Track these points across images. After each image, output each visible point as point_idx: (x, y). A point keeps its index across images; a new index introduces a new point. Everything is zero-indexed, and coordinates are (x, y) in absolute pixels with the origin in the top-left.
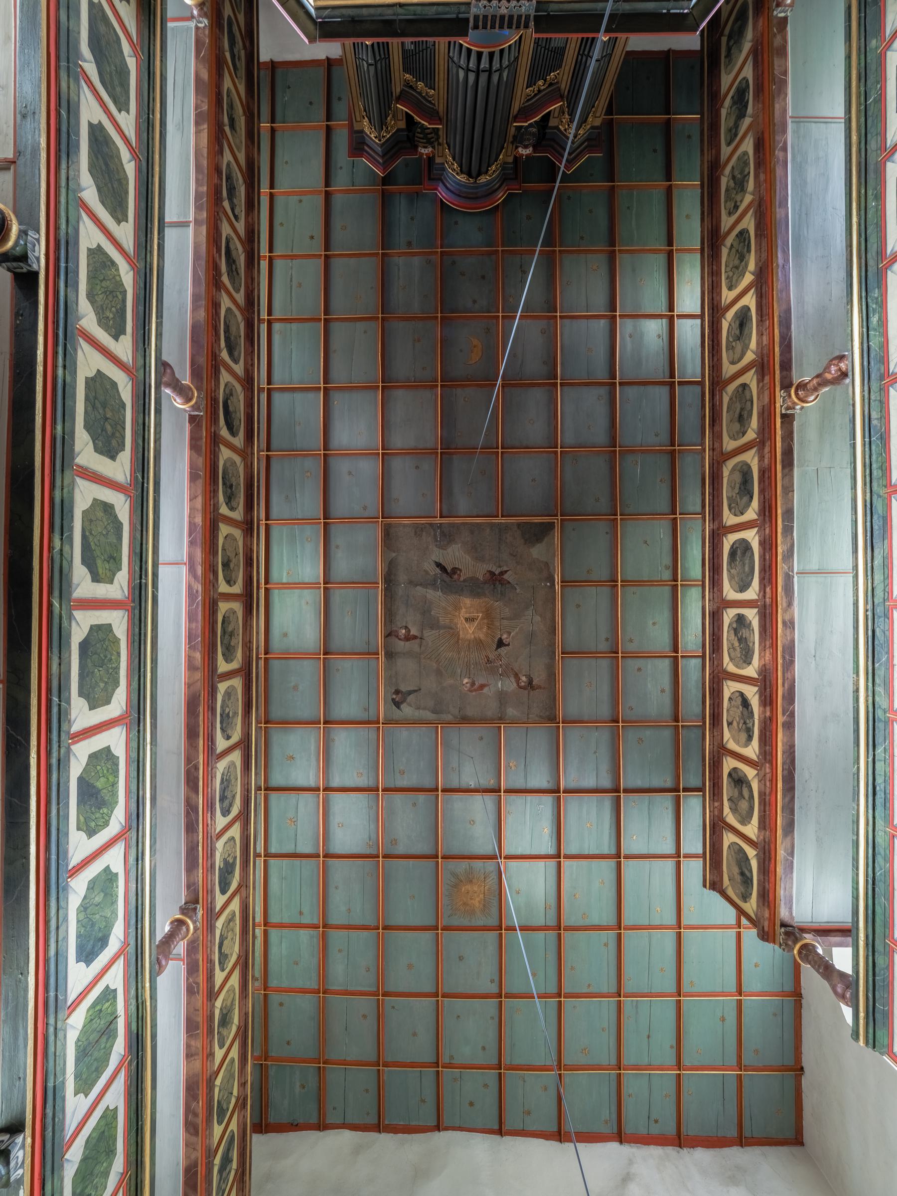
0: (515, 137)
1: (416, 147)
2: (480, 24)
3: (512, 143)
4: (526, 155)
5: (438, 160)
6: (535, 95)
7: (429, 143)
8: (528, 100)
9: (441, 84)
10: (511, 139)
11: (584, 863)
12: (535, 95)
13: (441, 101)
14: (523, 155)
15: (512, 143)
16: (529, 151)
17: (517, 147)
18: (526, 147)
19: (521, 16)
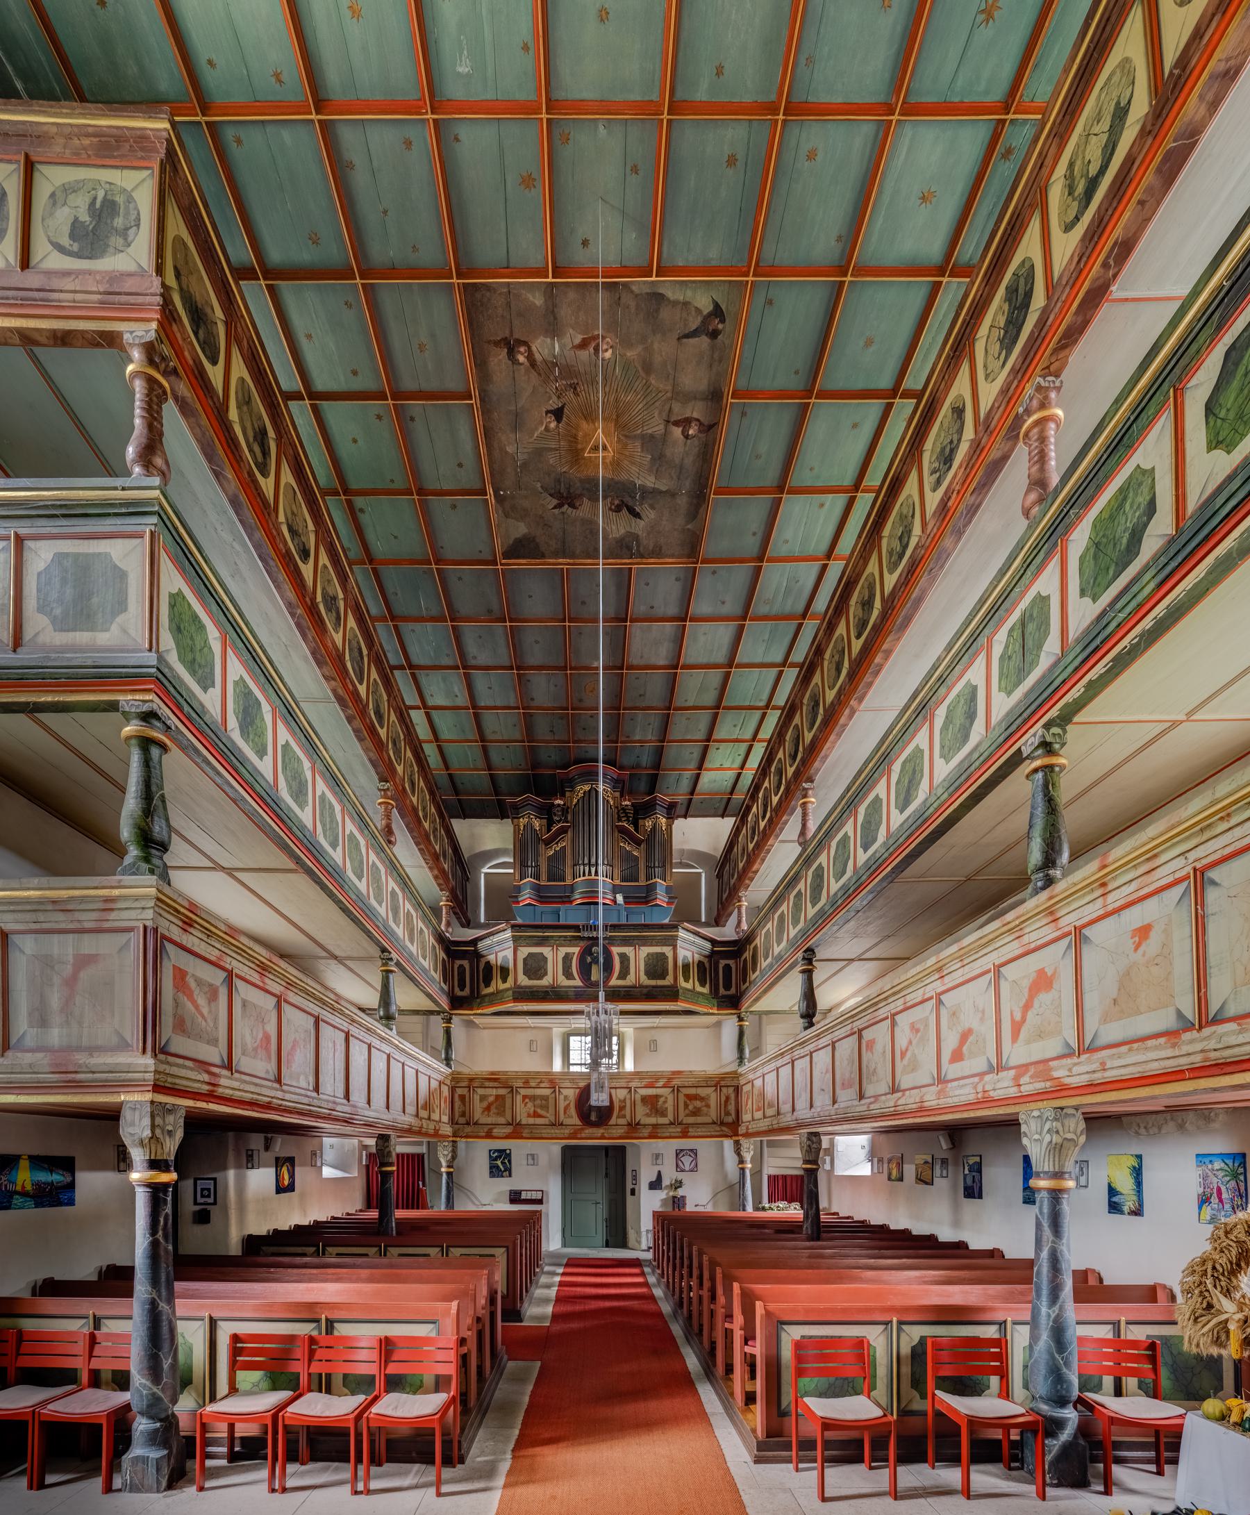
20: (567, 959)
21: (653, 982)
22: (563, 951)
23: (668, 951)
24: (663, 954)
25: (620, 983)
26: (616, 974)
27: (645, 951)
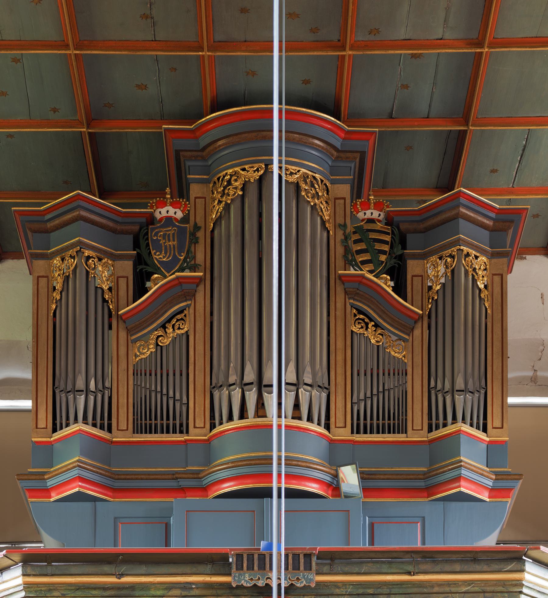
0: (195, 240)
1: (389, 221)
2: (302, 560)
3: (197, 228)
4: (164, 205)
5: (344, 190)
6: (169, 321)
7: (363, 232)
8: (181, 312)
9: (340, 344)
10: (200, 234)
11: (398, 524)
12: (169, 321)
13: (340, 313)
14: (173, 205)
15: (197, 228)
16: (163, 212)
17: (185, 219)
18: (169, 220)
19: (248, 569)
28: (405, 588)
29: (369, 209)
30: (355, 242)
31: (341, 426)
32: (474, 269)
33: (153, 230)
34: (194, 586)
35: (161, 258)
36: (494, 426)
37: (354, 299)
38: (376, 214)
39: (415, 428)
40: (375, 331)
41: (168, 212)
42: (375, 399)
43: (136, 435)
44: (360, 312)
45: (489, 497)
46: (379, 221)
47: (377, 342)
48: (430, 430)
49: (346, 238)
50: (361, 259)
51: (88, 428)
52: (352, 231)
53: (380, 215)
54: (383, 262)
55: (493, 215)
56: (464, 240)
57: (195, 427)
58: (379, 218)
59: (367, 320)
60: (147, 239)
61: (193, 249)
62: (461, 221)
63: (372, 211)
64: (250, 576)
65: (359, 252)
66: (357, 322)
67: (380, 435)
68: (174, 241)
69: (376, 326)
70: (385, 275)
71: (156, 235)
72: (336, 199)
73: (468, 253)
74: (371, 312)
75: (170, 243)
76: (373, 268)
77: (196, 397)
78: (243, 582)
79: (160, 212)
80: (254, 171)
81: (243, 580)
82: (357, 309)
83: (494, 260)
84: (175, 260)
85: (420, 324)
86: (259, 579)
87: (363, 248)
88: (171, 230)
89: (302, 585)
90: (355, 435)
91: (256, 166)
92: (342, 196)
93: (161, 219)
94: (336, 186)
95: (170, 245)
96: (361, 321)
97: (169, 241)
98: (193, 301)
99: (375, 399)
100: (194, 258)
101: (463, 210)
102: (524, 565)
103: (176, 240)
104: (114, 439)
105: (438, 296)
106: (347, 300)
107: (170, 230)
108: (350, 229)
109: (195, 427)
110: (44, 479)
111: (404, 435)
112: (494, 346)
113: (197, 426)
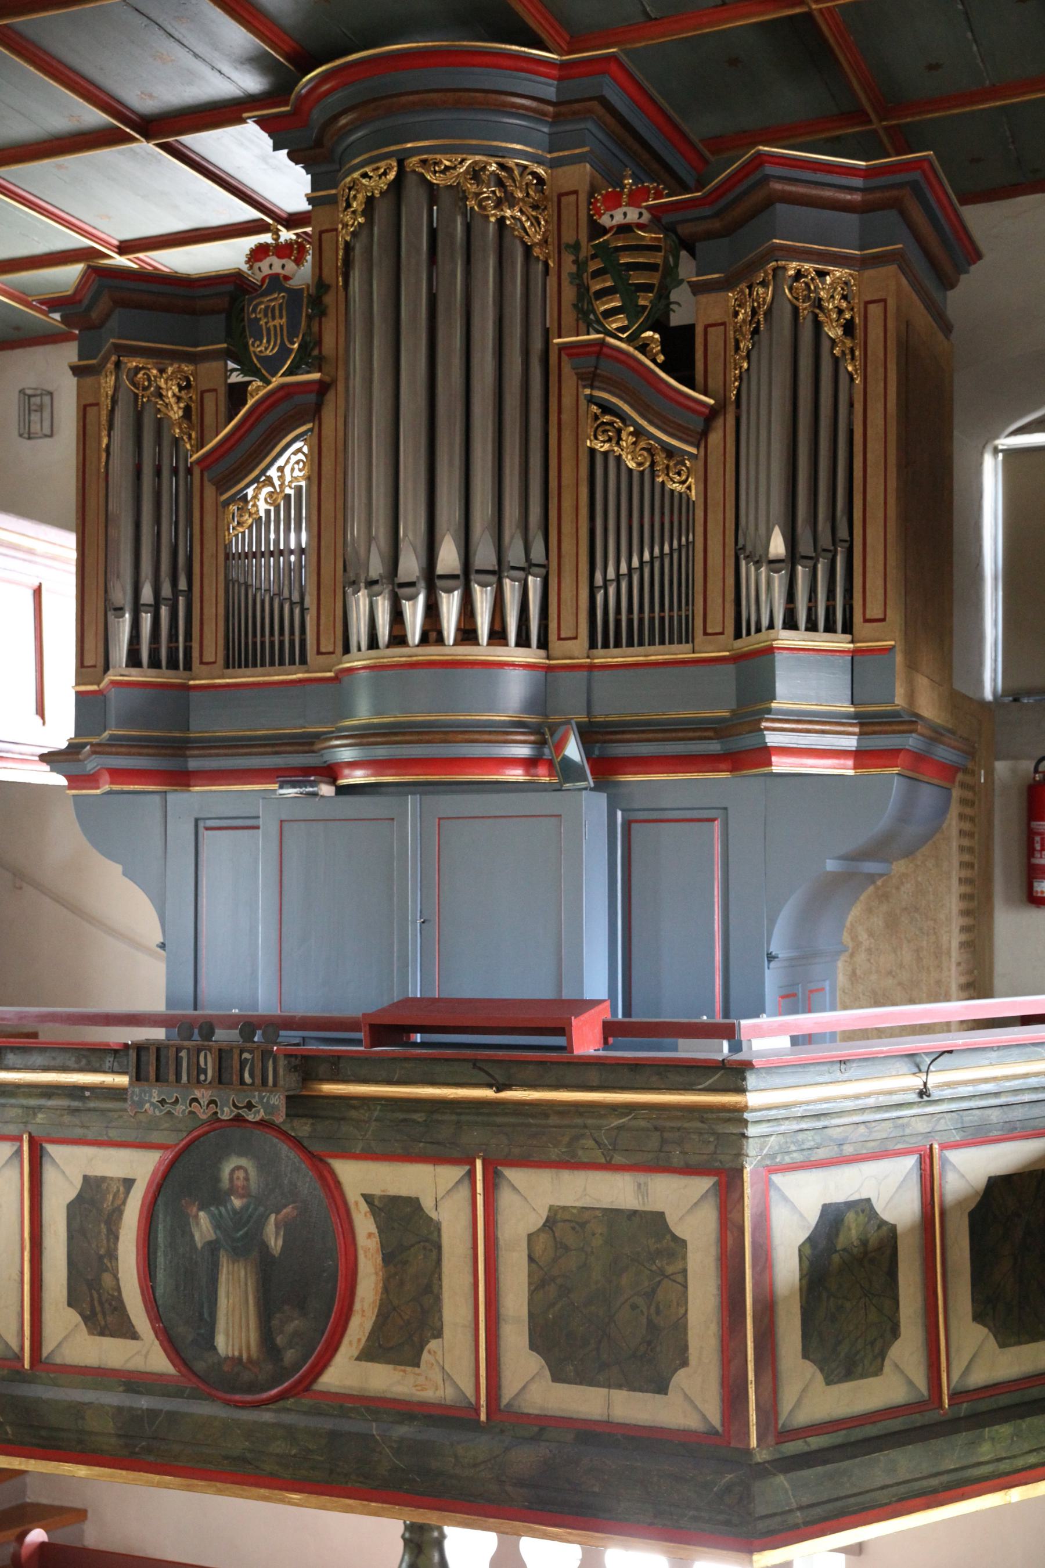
20: (94, 1205)
21: (586, 1402)
22: (70, 1167)
23: (680, 1200)
24: (655, 1223)
25: (384, 1380)
26: (360, 1327)
27: (534, 1195)
28: (489, 1115)
29: (620, 206)
30: (596, 274)
31: (569, 635)
32: (818, 303)
33: (251, 300)
34: (87, 1094)
35: (261, 352)
36: (868, 616)
37: (592, 387)
38: (632, 215)
39: (709, 631)
40: (634, 443)
41: (271, 266)
42: (612, 590)
43: (230, 671)
44: (607, 408)
45: (855, 768)
46: (641, 227)
47: (640, 464)
48: (738, 635)
49: (581, 265)
50: (602, 309)
51: (135, 675)
52: (590, 254)
53: (641, 214)
54: (645, 307)
55: (859, 182)
56: (782, 247)
57: (319, 653)
58: (641, 221)
59: (619, 424)
60: (243, 320)
61: (315, 329)
62: (780, 207)
63: (624, 209)
64: (159, 1095)
65: (601, 294)
66: (600, 429)
67: (636, 649)
68: (281, 317)
69: (639, 433)
70: (650, 333)
71: (254, 310)
72: (560, 196)
73: (799, 271)
74: (626, 408)
75: (277, 322)
76: (626, 323)
77: (322, 597)
78: (147, 1106)
79: (260, 269)
80: (380, 176)
81: (147, 1102)
82: (599, 406)
83: (869, 273)
84: (284, 352)
85: (720, 422)
86: (177, 1101)
87: (609, 284)
88: (277, 299)
89: (258, 1118)
90: (600, 651)
91: (383, 165)
92: (572, 189)
93: (263, 280)
94: (560, 171)
95: (275, 326)
96: (608, 427)
97: (274, 319)
98: (317, 423)
99: (612, 590)
100: (319, 343)
101: (778, 186)
102: (744, 1079)
103: (284, 313)
104: (191, 682)
105: (749, 363)
106: (580, 389)
107: (275, 299)
108: (585, 251)
109: (319, 653)
110: (79, 760)
111: (689, 646)
112: (869, 450)
113: (323, 650)
